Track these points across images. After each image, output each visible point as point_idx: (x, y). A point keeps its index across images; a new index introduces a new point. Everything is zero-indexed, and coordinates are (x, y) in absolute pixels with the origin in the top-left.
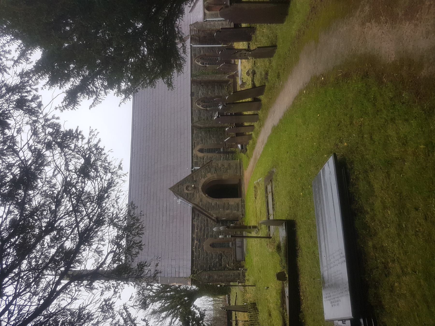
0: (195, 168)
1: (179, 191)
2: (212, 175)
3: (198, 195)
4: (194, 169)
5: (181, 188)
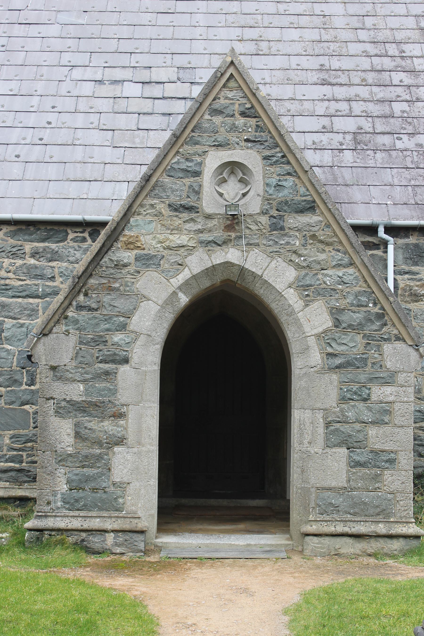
0: (391, 248)
1: (218, 120)
2: (318, 336)
3: (184, 239)
4: (385, 244)
5: (233, 128)
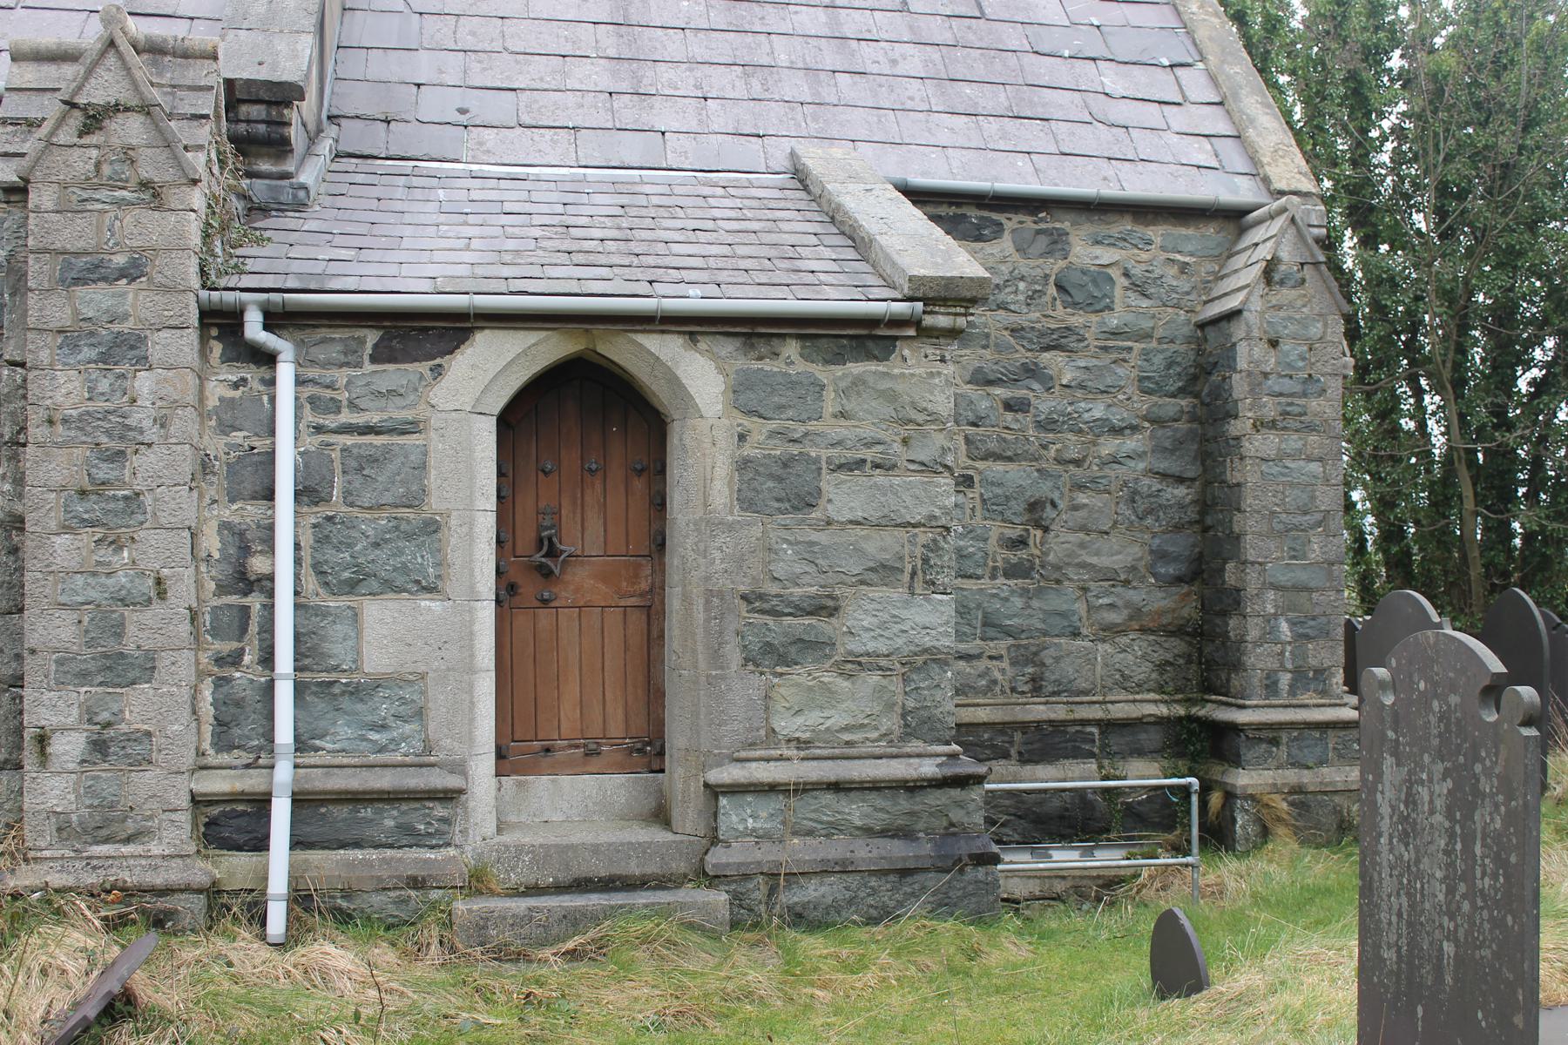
0: (285, 373)
